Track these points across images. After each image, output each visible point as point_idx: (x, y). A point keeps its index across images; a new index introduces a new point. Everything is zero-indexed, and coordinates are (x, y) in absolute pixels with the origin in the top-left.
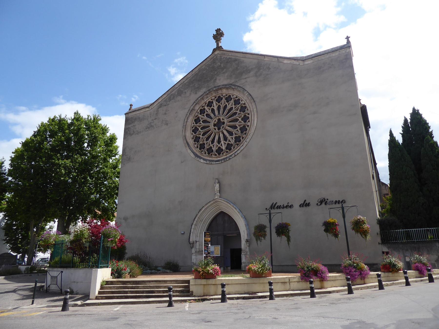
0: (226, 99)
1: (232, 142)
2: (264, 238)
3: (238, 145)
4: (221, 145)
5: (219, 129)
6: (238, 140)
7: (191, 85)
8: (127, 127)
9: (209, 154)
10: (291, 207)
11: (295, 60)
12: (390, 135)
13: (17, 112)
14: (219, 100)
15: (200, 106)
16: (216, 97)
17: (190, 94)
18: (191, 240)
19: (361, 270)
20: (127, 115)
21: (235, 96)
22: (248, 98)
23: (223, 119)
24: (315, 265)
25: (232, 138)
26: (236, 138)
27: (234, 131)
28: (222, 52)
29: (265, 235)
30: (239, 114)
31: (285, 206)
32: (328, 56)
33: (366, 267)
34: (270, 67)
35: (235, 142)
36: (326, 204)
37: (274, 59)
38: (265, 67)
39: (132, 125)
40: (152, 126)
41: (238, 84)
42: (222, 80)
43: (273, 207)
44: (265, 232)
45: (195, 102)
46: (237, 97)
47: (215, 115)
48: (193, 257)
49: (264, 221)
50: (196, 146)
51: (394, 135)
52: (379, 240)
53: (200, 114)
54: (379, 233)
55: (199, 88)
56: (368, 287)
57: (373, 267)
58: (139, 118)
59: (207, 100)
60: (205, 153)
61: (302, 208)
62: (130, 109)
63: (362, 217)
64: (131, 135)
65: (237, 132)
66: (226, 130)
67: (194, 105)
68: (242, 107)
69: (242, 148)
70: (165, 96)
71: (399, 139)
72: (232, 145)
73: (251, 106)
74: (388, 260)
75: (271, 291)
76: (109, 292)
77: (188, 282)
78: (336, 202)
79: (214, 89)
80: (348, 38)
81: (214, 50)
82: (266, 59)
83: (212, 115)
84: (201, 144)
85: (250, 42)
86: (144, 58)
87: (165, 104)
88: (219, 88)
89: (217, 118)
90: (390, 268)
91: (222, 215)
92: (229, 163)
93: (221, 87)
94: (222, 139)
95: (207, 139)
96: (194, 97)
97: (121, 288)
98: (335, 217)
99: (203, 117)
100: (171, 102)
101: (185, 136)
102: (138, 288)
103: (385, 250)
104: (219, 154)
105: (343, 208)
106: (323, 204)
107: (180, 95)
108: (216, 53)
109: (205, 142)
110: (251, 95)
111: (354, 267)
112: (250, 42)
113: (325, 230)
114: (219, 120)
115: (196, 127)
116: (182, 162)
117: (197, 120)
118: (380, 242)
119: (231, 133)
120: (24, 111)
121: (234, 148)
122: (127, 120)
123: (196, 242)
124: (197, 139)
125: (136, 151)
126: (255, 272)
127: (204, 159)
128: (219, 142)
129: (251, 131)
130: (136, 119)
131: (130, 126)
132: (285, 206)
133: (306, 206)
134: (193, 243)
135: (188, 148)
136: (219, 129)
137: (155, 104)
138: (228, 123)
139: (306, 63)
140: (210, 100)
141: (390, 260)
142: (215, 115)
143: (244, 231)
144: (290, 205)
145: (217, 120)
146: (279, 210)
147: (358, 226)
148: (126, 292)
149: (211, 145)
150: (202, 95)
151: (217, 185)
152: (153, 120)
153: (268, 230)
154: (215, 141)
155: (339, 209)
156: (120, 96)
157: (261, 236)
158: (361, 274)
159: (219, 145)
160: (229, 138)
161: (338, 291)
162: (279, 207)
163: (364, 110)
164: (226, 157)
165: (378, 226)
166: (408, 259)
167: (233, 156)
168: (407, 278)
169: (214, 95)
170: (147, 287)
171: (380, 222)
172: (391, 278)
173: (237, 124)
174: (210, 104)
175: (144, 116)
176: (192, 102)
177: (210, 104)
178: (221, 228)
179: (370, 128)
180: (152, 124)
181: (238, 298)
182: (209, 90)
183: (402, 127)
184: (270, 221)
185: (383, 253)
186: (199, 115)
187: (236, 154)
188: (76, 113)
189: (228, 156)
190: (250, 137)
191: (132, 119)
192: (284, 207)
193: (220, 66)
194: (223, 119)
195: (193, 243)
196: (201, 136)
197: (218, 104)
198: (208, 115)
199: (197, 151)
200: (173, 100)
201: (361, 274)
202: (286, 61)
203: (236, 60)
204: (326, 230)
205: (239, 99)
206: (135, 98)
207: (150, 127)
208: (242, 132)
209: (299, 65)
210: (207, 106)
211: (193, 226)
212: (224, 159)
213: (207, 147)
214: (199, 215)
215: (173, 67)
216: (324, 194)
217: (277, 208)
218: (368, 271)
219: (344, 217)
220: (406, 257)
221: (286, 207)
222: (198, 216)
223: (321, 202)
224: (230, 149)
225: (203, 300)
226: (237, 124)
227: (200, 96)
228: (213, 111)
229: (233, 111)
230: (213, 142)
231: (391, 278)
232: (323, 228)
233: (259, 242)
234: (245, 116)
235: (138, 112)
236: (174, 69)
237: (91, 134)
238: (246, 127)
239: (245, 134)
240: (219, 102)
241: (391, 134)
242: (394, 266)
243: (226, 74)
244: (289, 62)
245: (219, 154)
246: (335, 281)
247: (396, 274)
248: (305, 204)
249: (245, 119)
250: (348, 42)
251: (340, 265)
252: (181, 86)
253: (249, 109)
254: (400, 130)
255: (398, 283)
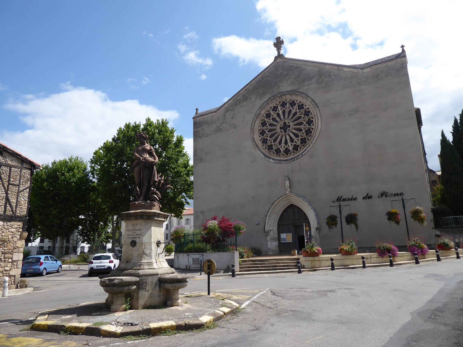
0: (290, 104)
1: (299, 143)
2: (336, 226)
3: (304, 146)
4: (288, 146)
5: (285, 131)
6: (304, 141)
7: (256, 91)
8: (196, 130)
9: (277, 154)
10: (355, 199)
11: (354, 68)
12: (442, 136)
13: (25, 102)
14: (283, 105)
15: (265, 111)
16: (280, 103)
17: (256, 99)
18: (266, 229)
19: (422, 249)
20: (195, 119)
21: (298, 102)
22: (311, 103)
23: (288, 123)
24: (389, 246)
25: (298, 140)
26: (301, 139)
27: (300, 133)
28: (284, 60)
29: (337, 223)
30: (303, 118)
31: (350, 198)
32: (385, 65)
33: (426, 246)
34: (331, 74)
35: (301, 143)
36: (386, 196)
37: (334, 67)
38: (325, 74)
39: (201, 128)
40: (220, 129)
41: (301, 91)
42: (285, 87)
43: (339, 199)
44: (336, 221)
45: (260, 107)
46: (300, 103)
47: (281, 119)
48: (269, 243)
49: (336, 212)
50: (264, 147)
51: (446, 136)
52: (433, 225)
53: (266, 118)
54: (433, 220)
55: (264, 94)
56: (428, 261)
57: (430, 247)
58: (207, 122)
59: (272, 105)
60: (274, 153)
61: (365, 200)
62: (196, 113)
63: (419, 208)
64: (200, 137)
65: (302, 134)
66: (292, 133)
67: (260, 110)
68: (305, 111)
69: (309, 149)
70: (231, 101)
71: (450, 138)
72: (298, 146)
73: (314, 111)
74: (442, 241)
75: (364, 263)
76: (246, 267)
77: (298, 259)
78: (395, 195)
79: (279, 95)
80: (403, 47)
81: (276, 58)
82: (327, 67)
83: (278, 119)
84: (269, 146)
85: (264, 10)
86: (151, 35)
87: (232, 109)
88: (283, 94)
89: (283, 121)
90: (444, 247)
91: (292, 207)
92: (297, 162)
93: (284, 93)
94: (289, 141)
95: (275, 141)
96: (259, 103)
97: (250, 264)
98: (397, 208)
99: (269, 121)
100: (237, 107)
101: (254, 138)
102: (264, 264)
103: (438, 233)
104: (287, 154)
105: (403, 201)
106: (384, 196)
107: (246, 101)
108: (279, 60)
109: (273, 143)
110: (314, 101)
111: (417, 247)
112: (264, 10)
113: (388, 219)
114: (285, 123)
115: (263, 130)
116: (252, 162)
117: (264, 124)
118: (434, 227)
119: (297, 136)
120: (31, 100)
121: (300, 148)
122: (195, 124)
123: (271, 230)
124: (264, 141)
125: (207, 152)
126: (346, 251)
127: (273, 159)
128: (286, 143)
129: (316, 133)
130: (204, 123)
131: (199, 129)
132: (350, 198)
133: (368, 198)
134: (268, 232)
135: (257, 149)
136: (285, 131)
137: (222, 109)
138: (294, 127)
139: (365, 71)
140: (274, 105)
141: (444, 241)
142: (280, 119)
143: (313, 221)
144: (354, 198)
145: (283, 124)
146: (344, 202)
147: (416, 215)
148: (258, 267)
149: (279, 146)
150: (267, 101)
151: (288, 182)
152: (221, 124)
153: (338, 219)
154: (283, 142)
155: (399, 201)
156: (130, 79)
157: (333, 225)
158: (422, 251)
159: (287, 146)
160: (295, 139)
161: (406, 264)
162: (344, 200)
163: (418, 112)
164: (293, 157)
165: (432, 214)
166: (457, 241)
167: (301, 156)
168: (457, 254)
169: (278, 100)
170: (270, 263)
171: (433, 211)
172: (445, 254)
173: (302, 127)
174: (275, 109)
175: (212, 120)
176: (258, 107)
177: (275, 109)
178: (292, 219)
179: (422, 125)
180: (221, 127)
181: (341, 268)
182: (274, 96)
183: (453, 127)
184: (340, 213)
185: (436, 236)
186: (265, 119)
187: (303, 154)
188: (148, 120)
189: (295, 156)
190: (315, 139)
191: (200, 124)
192: (349, 200)
193: (283, 73)
194: (288, 123)
195: (268, 232)
196: (268, 138)
197: (283, 109)
198: (274, 119)
199: (266, 152)
200: (239, 105)
201: (422, 251)
202: (345, 69)
203: (297, 68)
204: (389, 219)
205: (303, 105)
206: (145, 81)
207: (218, 130)
208: (307, 134)
209: (358, 72)
210: (273, 110)
211: (267, 217)
212: (292, 159)
213: (274, 148)
214: (272, 208)
215: (183, 44)
216: (385, 188)
217: (343, 200)
218: (427, 249)
219: (404, 207)
220: (456, 239)
221: (351, 199)
222: (271, 209)
223: (382, 195)
224: (297, 150)
225: (315, 270)
226: (302, 127)
227: (266, 102)
228: (278, 115)
229: (298, 115)
230: (280, 143)
231: (445, 254)
232: (387, 217)
233: (331, 229)
234: (309, 119)
235: (205, 116)
236: (184, 46)
237: (164, 138)
238: (311, 130)
239: (310, 136)
240: (284, 107)
241: (443, 135)
242: (447, 245)
243: (289, 81)
244: (348, 70)
245: (287, 154)
246: (403, 257)
247: (448, 252)
248: (368, 197)
249: (310, 122)
250: (403, 51)
251: (406, 246)
252: (246, 92)
253: (313, 113)
254: (451, 129)
255: (450, 258)
